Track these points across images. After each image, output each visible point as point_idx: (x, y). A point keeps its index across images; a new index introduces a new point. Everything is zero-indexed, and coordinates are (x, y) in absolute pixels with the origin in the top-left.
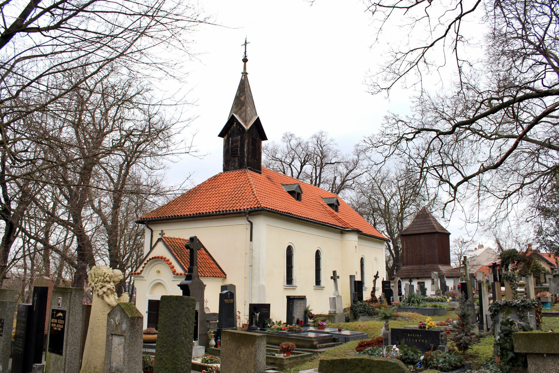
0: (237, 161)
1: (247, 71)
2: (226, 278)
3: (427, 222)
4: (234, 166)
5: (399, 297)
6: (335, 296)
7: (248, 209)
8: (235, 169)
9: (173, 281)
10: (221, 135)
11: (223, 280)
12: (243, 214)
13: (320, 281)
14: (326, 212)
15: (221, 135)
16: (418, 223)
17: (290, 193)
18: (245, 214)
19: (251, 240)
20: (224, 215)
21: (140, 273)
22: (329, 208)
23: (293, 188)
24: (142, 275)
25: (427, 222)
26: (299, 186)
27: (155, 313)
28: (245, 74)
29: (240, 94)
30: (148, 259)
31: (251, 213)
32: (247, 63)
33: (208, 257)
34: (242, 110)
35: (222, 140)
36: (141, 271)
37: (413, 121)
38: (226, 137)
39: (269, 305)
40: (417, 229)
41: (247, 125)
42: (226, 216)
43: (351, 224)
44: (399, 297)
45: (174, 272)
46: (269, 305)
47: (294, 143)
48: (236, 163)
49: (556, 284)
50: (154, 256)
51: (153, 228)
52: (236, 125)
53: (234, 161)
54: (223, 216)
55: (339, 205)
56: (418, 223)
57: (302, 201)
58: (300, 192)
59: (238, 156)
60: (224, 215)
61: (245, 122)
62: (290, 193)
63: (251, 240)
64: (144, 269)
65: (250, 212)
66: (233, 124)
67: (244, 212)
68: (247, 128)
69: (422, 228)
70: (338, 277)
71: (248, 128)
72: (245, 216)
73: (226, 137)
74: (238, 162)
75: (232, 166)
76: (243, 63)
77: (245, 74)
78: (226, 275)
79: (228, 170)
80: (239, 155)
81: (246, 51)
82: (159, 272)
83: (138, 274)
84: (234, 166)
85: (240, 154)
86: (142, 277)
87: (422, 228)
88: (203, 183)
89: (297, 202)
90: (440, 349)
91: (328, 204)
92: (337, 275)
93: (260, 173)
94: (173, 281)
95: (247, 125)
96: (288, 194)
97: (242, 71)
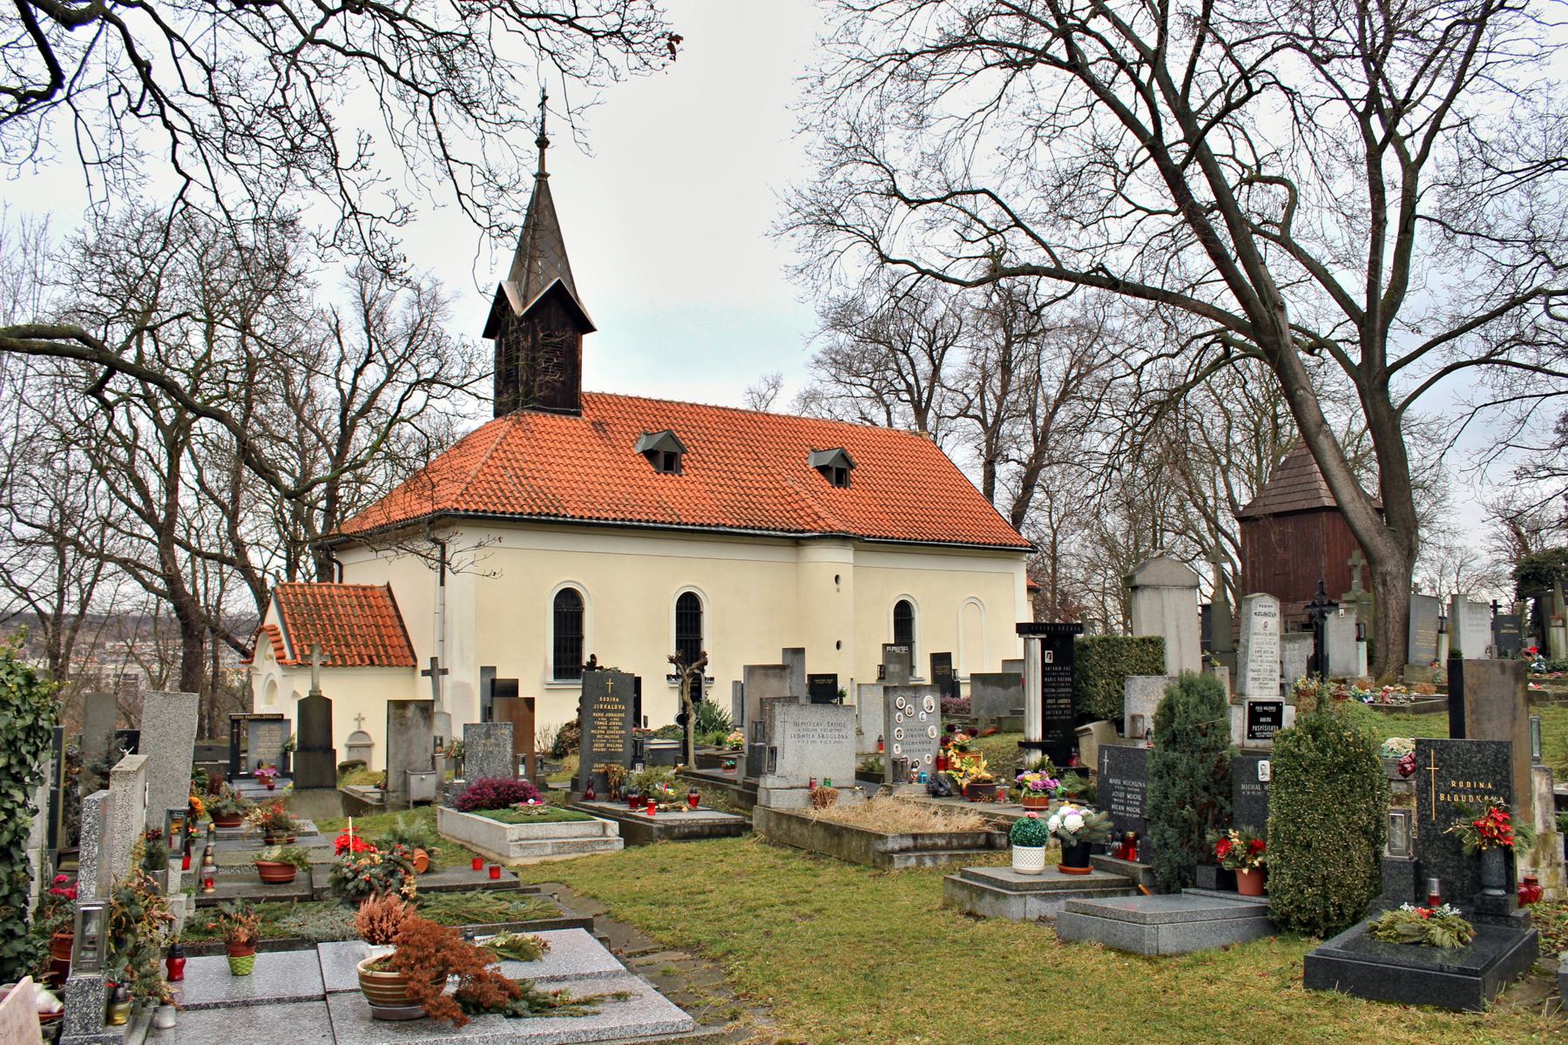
1: (547, 170)
3: (1304, 479)
16: (1282, 483)
17: (823, 470)
19: (442, 583)
23: (827, 459)
25: (1304, 479)
26: (843, 455)
28: (542, 177)
31: (438, 523)
37: (1326, 204)
40: (1278, 499)
47: (825, 358)
49: (449, 1000)
55: (852, 467)
56: (1282, 483)
62: (823, 470)
63: (442, 583)
65: (431, 522)
69: (1290, 498)
87: (1290, 498)
89: (840, 491)
96: (818, 475)
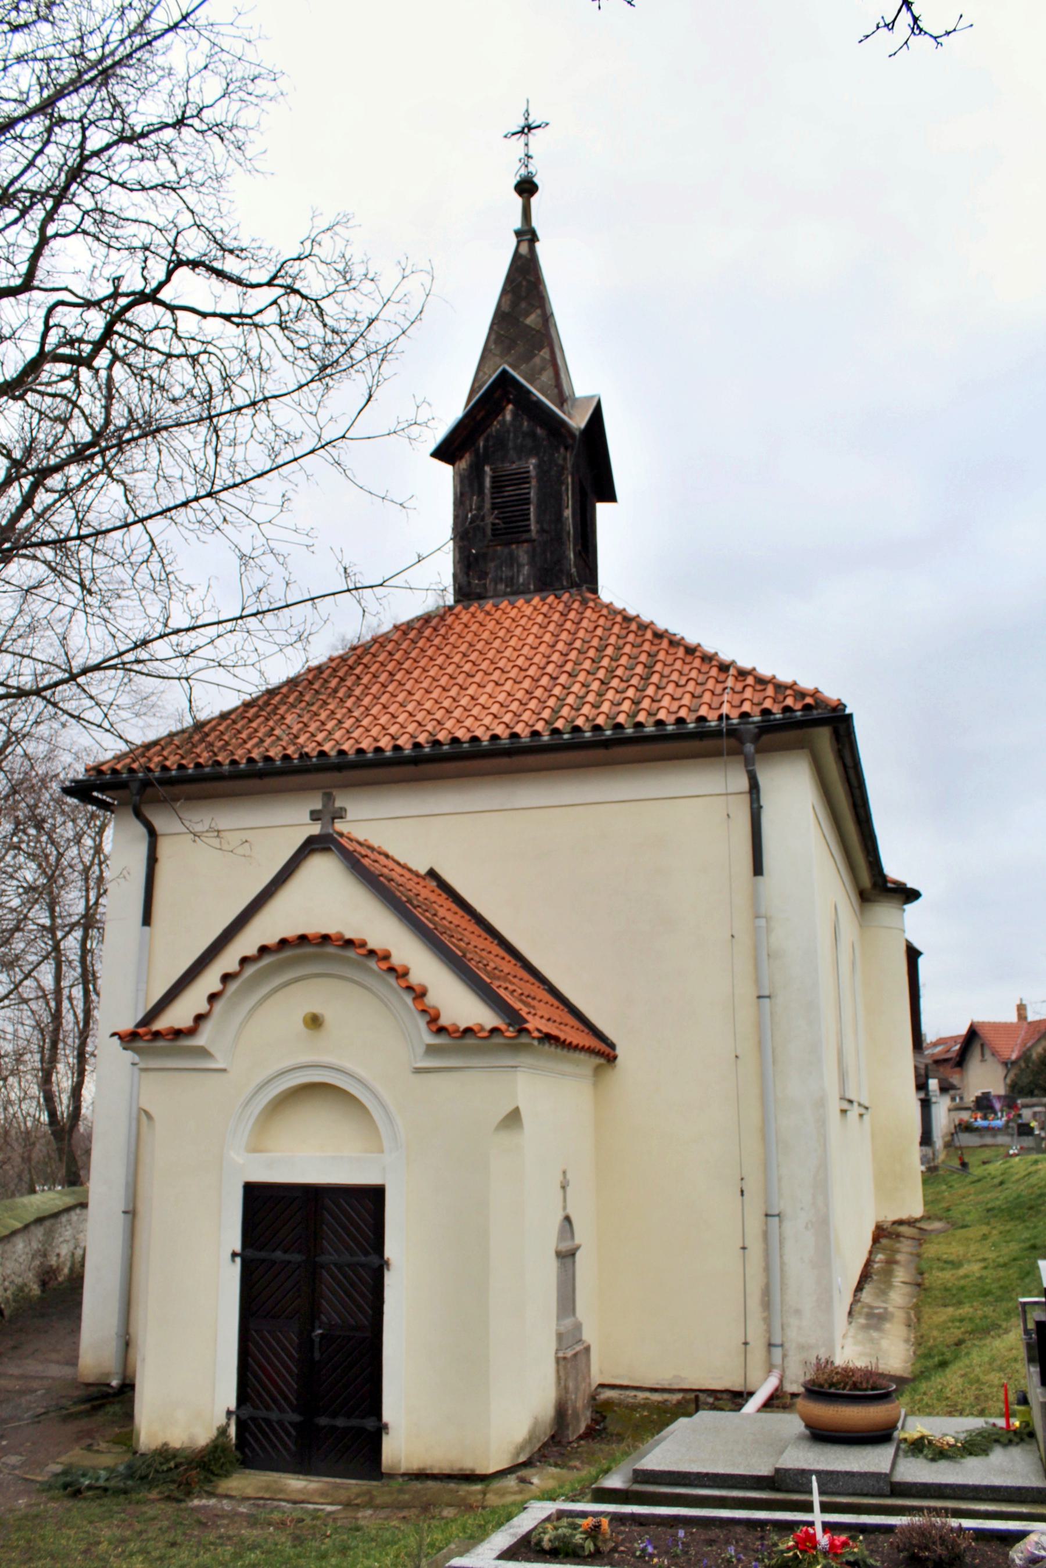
0: (524, 559)
4: (510, 581)
8: (516, 591)
9: (418, 1071)
10: (444, 452)
11: (597, 1070)
12: (725, 743)
15: (444, 452)
18: (733, 742)
20: (607, 744)
21: (191, 1032)
24: (200, 1040)
27: (297, 1258)
28: (527, 235)
29: (514, 304)
30: (246, 943)
32: (534, 200)
34: (537, 360)
35: (445, 473)
36: (199, 1018)
38: (463, 464)
39: (375, 1196)
45: (433, 1018)
46: (375, 1196)
48: (520, 566)
50: (290, 931)
51: (160, 823)
52: (515, 415)
53: (512, 561)
54: (600, 753)
59: (530, 541)
60: (607, 744)
64: (219, 1006)
66: (502, 410)
71: (583, 425)
72: (734, 752)
73: (463, 464)
74: (532, 562)
75: (498, 580)
76: (518, 201)
77: (527, 235)
78: (612, 1046)
79: (481, 597)
80: (534, 534)
82: (315, 1022)
83: (178, 1034)
84: (510, 581)
86: (203, 1053)
88: (375, 640)
94: (418, 1071)
97: (518, 224)
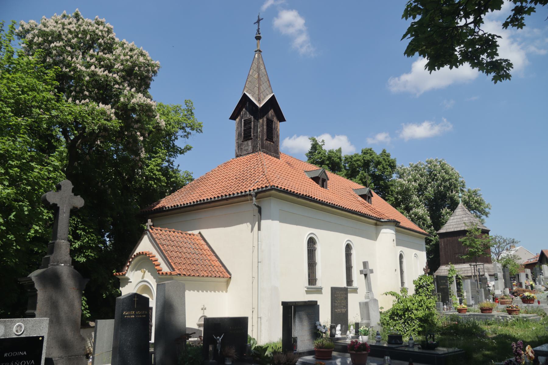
0: (250, 144)
2: (230, 278)
5: (458, 298)
6: (367, 300)
7: (254, 190)
13: (352, 281)
14: (358, 202)
22: (360, 199)
33: (210, 253)
41: (260, 104)
42: (230, 201)
43: (386, 215)
44: (458, 298)
57: (328, 189)
58: (325, 178)
61: (259, 101)
62: (313, 179)
67: (250, 195)
68: (260, 105)
70: (372, 271)
71: (261, 105)
74: (252, 145)
81: (259, 29)
85: (254, 136)
90: (17, 127)
91: (360, 195)
92: (370, 268)
93: (278, 158)
95: (260, 104)
